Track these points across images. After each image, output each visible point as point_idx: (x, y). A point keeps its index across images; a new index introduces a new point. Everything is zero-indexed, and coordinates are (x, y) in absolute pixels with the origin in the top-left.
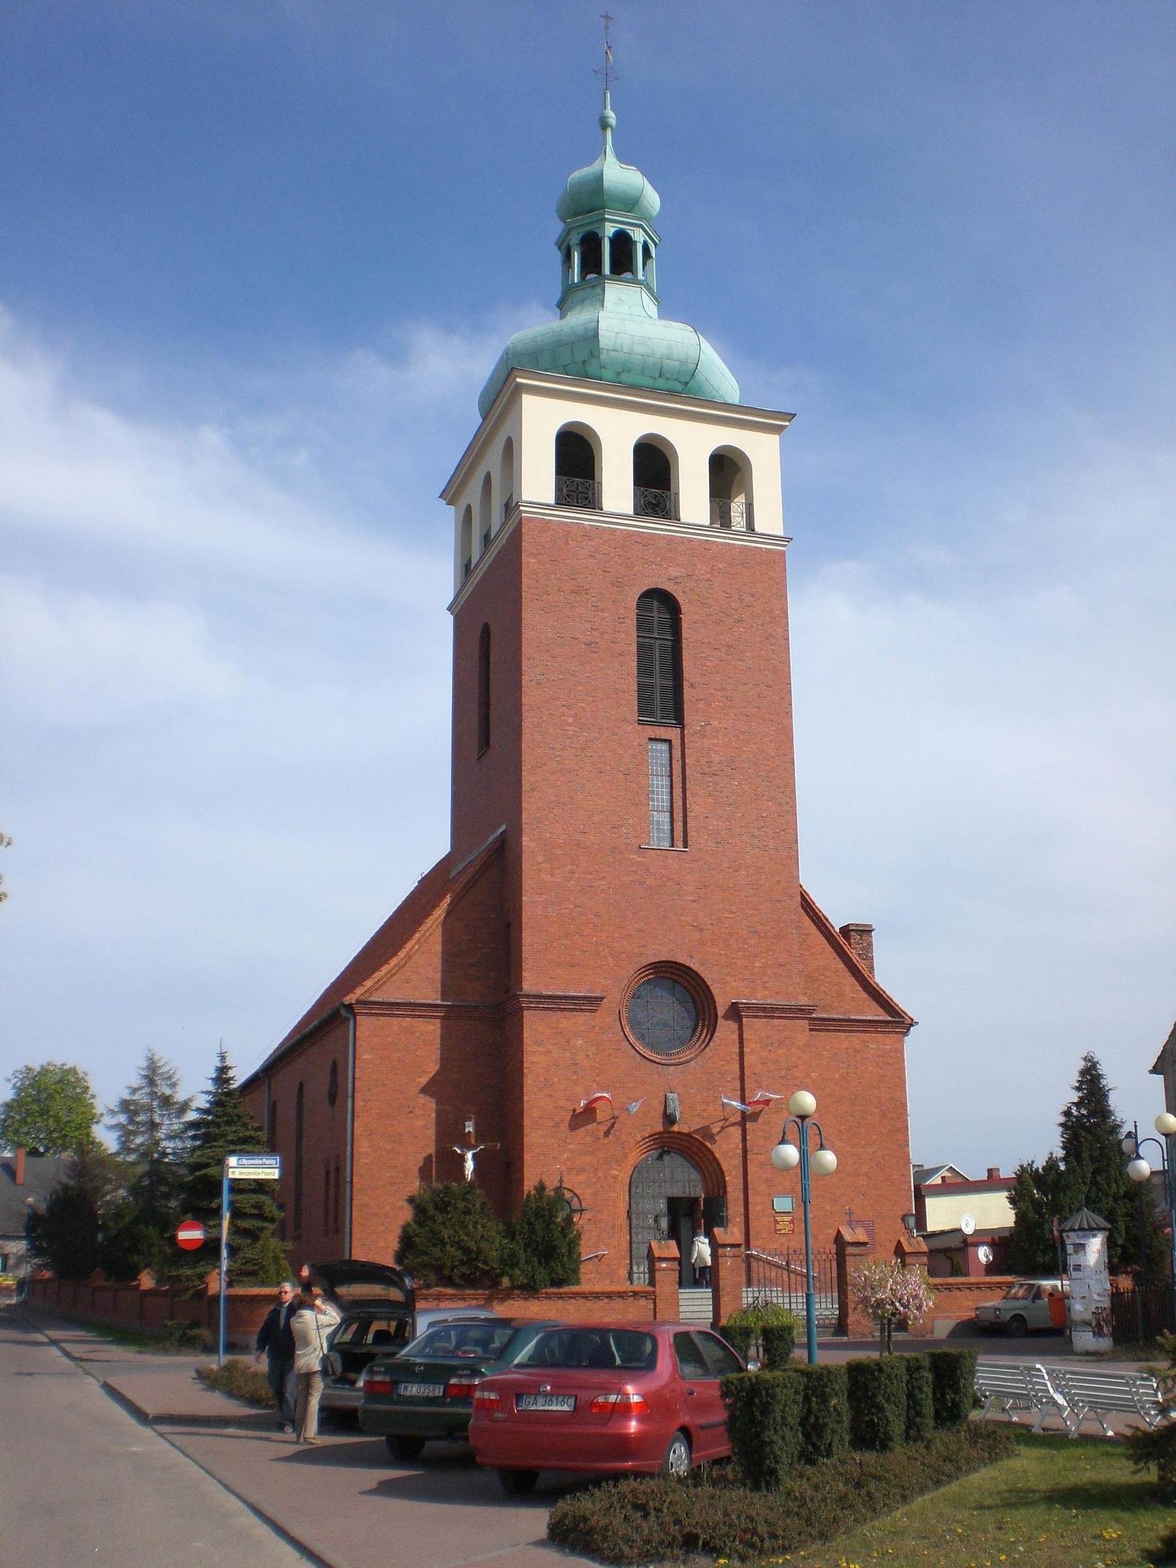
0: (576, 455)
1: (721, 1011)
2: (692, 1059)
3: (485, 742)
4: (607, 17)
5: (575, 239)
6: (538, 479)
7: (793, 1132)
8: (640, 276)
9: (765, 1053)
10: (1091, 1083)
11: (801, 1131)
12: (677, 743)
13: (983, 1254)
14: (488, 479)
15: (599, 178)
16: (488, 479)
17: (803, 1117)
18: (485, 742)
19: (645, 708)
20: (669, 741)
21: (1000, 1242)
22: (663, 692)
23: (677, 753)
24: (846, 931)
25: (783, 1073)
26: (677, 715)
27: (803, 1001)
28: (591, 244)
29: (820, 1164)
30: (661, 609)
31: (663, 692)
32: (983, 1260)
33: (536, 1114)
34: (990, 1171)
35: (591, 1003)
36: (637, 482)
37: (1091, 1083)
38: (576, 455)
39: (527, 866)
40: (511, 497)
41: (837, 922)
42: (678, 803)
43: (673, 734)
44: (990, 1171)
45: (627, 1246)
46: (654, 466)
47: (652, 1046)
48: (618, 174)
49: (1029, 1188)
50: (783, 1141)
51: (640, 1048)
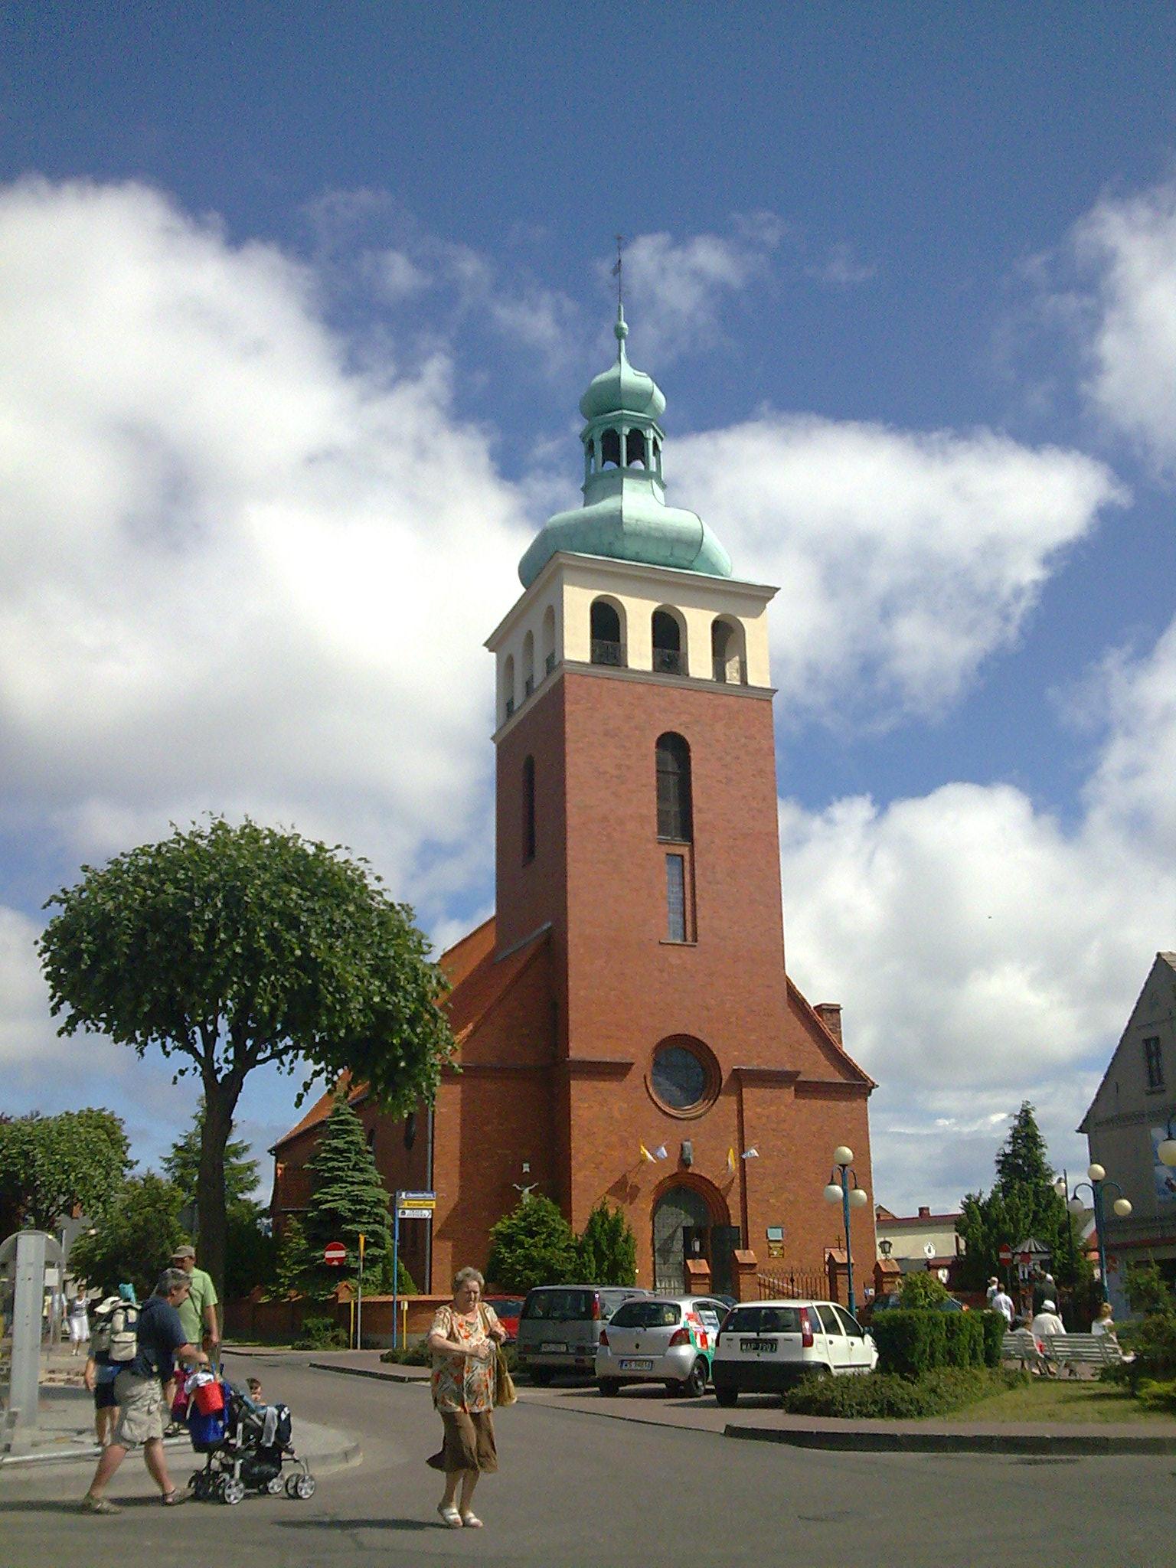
0: (607, 623)
1: (725, 1076)
2: (705, 1113)
3: (530, 851)
4: (619, 238)
5: (597, 435)
6: (577, 643)
7: (838, 1177)
8: (653, 468)
9: (759, 1110)
10: (1025, 1133)
11: (843, 1175)
12: (687, 858)
13: (943, 1275)
14: (530, 637)
15: (618, 380)
16: (530, 637)
17: (844, 1166)
18: (530, 851)
19: (662, 828)
20: (682, 856)
21: (955, 1266)
22: (678, 817)
23: (687, 865)
24: (819, 1008)
25: (774, 1126)
26: (686, 832)
27: (788, 1068)
28: (611, 440)
29: (857, 1197)
30: (674, 748)
31: (678, 817)
32: (944, 1280)
33: (581, 1158)
34: (921, 1210)
35: (618, 1070)
36: (655, 645)
37: (1025, 1133)
38: (607, 623)
39: (572, 956)
40: (552, 655)
41: (813, 1002)
42: (688, 908)
43: (685, 851)
44: (921, 1210)
45: (651, 1266)
46: (668, 633)
47: (669, 1103)
48: (629, 375)
49: (974, 1221)
50: (832, 1183)
51: (660, 1104)
